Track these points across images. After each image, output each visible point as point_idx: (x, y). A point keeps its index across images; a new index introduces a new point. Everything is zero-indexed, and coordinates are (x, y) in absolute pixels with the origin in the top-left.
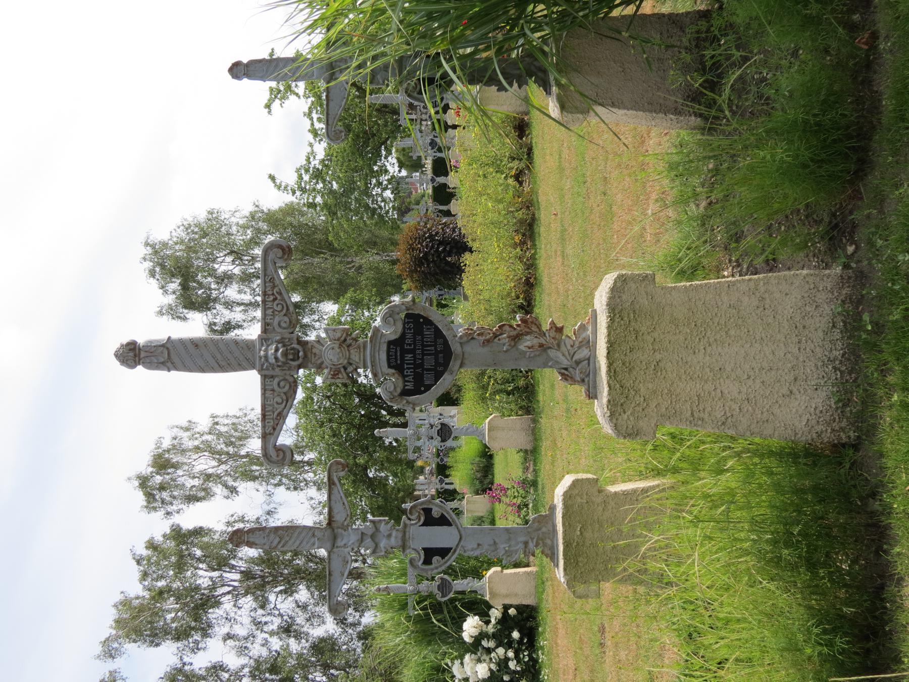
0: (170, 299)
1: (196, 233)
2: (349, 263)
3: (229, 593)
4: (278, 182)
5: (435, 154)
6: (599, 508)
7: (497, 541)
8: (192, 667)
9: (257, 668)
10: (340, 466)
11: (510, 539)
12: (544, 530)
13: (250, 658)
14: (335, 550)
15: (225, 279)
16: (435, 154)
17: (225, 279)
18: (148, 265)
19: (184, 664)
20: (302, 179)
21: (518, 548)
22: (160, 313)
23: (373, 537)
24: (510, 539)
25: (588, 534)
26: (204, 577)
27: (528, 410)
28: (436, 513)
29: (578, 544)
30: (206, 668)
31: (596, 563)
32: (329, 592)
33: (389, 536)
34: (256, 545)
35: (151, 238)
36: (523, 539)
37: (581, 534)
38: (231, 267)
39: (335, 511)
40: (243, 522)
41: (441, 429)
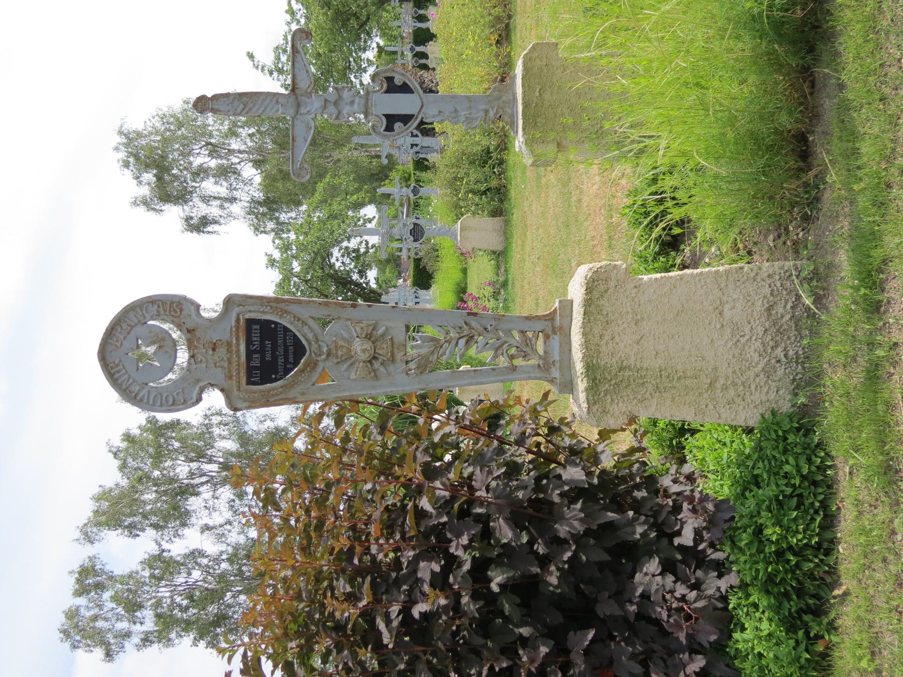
0: (145, 191)
1: (171, 123)
2: (327, 157)
3: (207, 482)
4: (256, 60)
5: (415, 24)
6: (559, 71)
7: (458, 108)
8: (170, 554)
9: (235, 555)
10: (304, 35)
11: (470, 108)
12: (504, 98)
13: (228, 545)
14: (298, 116)
15: (201, 173)
16: (415, 24)
17: (201, 173)
18: (122, 155)
19: (163, 551)
20: (280, 59)
21: (478, 115)
22: (135, 203)
23: (336, 104)
24: (470, 108)
25: (547, 96)
26: (182, 469)
27: (497, 213)
28: (398, 81)
29: (537, 104)
30: (185, 555)
31: (554, 124)
32: (293, 153)
33: (352, 103)
34: (220, 111)
35: (125, 126)
36: (483, 107)
37: (540, 95)
38: (207, 159)
39: (299, 78)
40: (221, 415)
41: (414, 229)
